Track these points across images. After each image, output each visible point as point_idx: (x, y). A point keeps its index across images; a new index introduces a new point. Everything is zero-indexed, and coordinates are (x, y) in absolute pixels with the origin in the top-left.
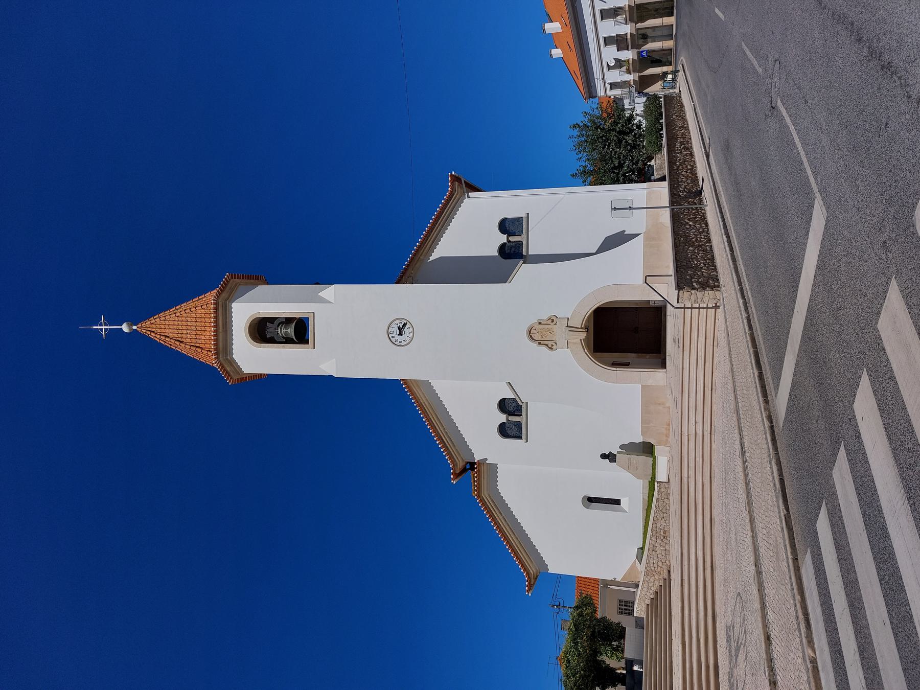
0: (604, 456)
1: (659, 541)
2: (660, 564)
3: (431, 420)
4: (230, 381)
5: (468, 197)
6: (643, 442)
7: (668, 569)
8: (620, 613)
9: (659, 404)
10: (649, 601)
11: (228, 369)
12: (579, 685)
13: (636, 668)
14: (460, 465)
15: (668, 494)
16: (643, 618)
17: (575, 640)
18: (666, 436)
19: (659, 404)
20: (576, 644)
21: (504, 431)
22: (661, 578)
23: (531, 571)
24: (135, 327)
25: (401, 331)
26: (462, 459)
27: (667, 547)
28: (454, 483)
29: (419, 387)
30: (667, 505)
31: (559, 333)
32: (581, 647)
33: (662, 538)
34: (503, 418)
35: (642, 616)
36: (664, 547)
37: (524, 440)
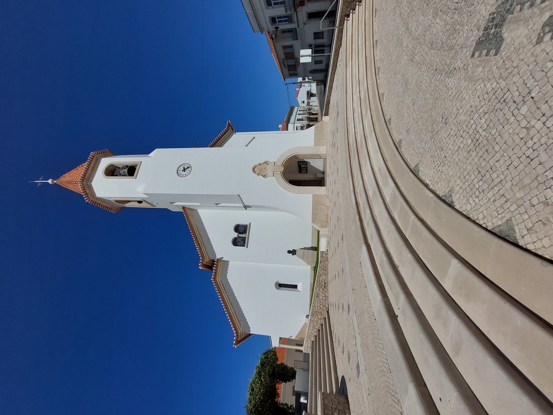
0: (289, 252)
1: (321, 290)
2: (322, 307)
3: (195, 233)
4: (87, 200)
5: (235, 134)
6: (312, 247)
7: (327, 310)
8: (293, 395)
9: (323, 205)
10: (314, 338)
11: (87, 191)
12: (258, 408)
13: (302, 400)
14: (207, 260)
15: (327, 258)
16: (309, 354)
17: (259, 373)
18: (326, 222)
19: (323, 205)
20: (260, 376)
21: (235, 242)
22: (322, 317)
23: (239, 331)
24: (55, 182)
25: (184, 170)
26: (209, 257)
27: (326, 294)
28: (200, 268)
29: (193, 217)
30: (327, 265)
31: (270, 170)
32: (263, 378)
33: (323, 287)
34: (236, 235)
35: (308, 352)
36: (325, 294)
37: (246, 247)
